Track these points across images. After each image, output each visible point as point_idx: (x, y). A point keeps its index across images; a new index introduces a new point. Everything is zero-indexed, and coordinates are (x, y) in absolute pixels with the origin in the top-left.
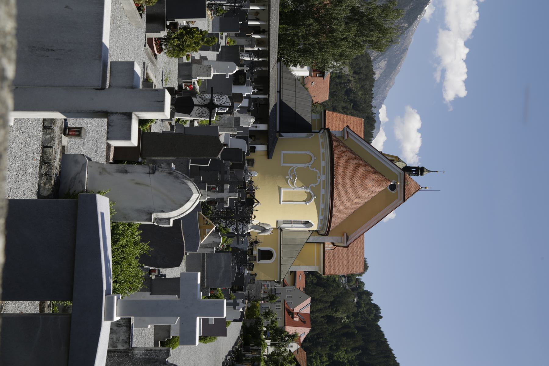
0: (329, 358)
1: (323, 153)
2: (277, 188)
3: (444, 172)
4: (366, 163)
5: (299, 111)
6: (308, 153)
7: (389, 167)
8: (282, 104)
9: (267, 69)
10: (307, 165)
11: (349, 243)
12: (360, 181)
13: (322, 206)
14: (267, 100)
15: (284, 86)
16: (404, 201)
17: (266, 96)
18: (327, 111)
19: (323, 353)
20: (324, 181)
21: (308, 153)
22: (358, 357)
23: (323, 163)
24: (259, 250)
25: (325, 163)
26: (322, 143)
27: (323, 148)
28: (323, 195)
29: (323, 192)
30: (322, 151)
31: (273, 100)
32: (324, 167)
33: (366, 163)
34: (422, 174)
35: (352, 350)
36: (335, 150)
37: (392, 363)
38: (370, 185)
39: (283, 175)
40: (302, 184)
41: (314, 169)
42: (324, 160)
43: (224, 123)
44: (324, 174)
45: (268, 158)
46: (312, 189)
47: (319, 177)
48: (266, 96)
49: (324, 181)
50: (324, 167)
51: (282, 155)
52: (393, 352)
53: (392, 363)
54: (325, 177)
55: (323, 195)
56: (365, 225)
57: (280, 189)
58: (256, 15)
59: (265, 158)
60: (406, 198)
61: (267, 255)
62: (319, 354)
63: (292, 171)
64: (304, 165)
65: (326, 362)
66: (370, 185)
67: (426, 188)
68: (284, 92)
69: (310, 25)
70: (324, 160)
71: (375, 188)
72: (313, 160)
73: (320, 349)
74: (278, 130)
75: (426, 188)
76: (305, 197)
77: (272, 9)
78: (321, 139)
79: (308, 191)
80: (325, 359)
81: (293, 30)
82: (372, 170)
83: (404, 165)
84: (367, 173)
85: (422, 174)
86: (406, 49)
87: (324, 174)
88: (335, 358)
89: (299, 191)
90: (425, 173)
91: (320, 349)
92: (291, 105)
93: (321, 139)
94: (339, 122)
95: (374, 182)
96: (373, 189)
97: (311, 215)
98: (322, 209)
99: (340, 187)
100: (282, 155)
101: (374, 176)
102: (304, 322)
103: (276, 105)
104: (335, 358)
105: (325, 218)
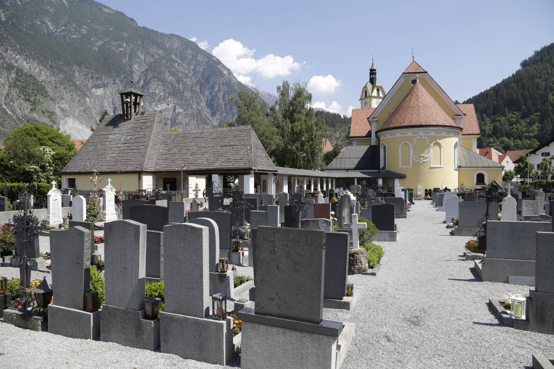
0: (491, 137)
1: (401, 134)
3: (373, 55)
5: (361, 156)
6: (400, 147)
9: (334, 179)
10: (411, 147)
11: (462, 114)
14: (360, 180)
15: (343, 167)
17: (356, 180)
19: (487, 141)
20: (424, 133)
22: (489, 116)
23: (421, 134)
24: (476, 184)
25: (409, 133)
27: (395, 135)
29: (433, 134)
30: (398, 135)
31: (358, 174)
32: (412, 133)
34: (375, 70)
35: (483, 121)
36: (397, 125)
37: (491, 92)
38: (422, 97)
39: (419, 165)
40: (427, 150)
41: (415, 141)
42: (406, 134)
43: (532, 210)
44: (418, 133)
45: (405, 177)
47: (421, 137)
48: (356, 180)
49: (424, 133)
51: (411, 164)
52: (483, 91)
53: (491, 92)
54: (421, 132)
55: (435, 133)
56: (447, 102)
57: (431, 168)
59: (405, 180)
62: (488, 144)
64: (411, 149)
65: (494, 139)
66: (422, 97)
67: (413, 57)
68: (347, 167)
71: (422, 94)
72: (407, 142)
73: (484, 144)
74: (377, 171)
76: (437, 147)
78: (387, 138)
79: (432, 145)
81: (300, 161)
82: (409, 96)
83: (369, 83)
84: (413, 100)
85: (375, 70)
86: (269, 94)
87: (418, 133)
88: (491, 133)
89: (432, 153)
90: (374, 68)
91: (484, 144)
92: (356, 161)
93: (387, 138)
94: (357, 126)
95: (419, 94)
96: (425, 95)
97: (450, 143)
98: (446, 134)
99: (428, 120)
101: (414, 95)
102: (487, 153)
103: (361, 172)
104: (491, 133)
105: (452, 132)
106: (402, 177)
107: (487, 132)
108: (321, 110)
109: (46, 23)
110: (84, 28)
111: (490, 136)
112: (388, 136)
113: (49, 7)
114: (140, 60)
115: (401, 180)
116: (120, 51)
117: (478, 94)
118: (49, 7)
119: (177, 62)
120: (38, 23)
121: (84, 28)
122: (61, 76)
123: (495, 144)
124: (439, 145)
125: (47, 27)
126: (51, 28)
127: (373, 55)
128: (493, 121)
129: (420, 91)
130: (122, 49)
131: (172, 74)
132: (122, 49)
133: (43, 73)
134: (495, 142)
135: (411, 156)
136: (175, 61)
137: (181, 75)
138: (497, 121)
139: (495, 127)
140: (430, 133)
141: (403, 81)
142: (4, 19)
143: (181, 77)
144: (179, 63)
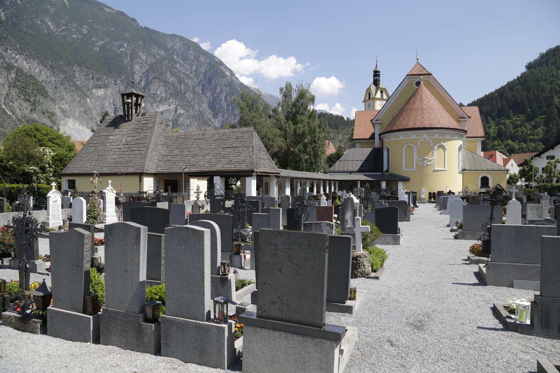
0: (495, 140)
1: (404, 137)
2: (434, 173)
3: (377, 56)
4: (408, 102)
6: (404, 149)
7: (401, 90)
8: (360, 171)
10: (415, 150)
12: (425, 107)
13: (448, 137)
14: (363, 182)
15: (346, 169)
16: (431, 74)
17: (359, 182)
18: (354, 138)
19: (492, 144)
20: (428, 136)
21: (404, 149)
22: (493, 119)
23: (425, 136)
24: (481, 188)
25: (413, 135)
26: (394, 138)
28: (440, 136)
29: (437, 136)
30: (402, 138)
31: (361, 177)
32: (416, 136)
33: (408, 102)
34: (379, 72)
36: (401, 128)
38: (426, 99)
39: (423, 168)
40: (431, 152)
41: (418, 143)
42: (410, 136)
43: (537, 214)
44: (422, 136)
45: (409, 180)
46: (435, 145)
47: (425, 139)
48: (359, 182)
49: (428, 136)
50: (416, 136)
51: (407, 170)
52: (487, 94)
54: (425, 135)
57: (435, 171)
58: (281, 189)
59: (408, 183)
60: (427, 73)
61: (485, 181)
63: (420, 161)
64: (415, 152)
65: (498, 142)
66: (426, 99)
68: (350, 169)
69: (300, 151)
70: (410, 136)
72: (411, 145)
74: (381, 173)
75: (418, 59)
76: (441, 150)
77: (309, 177)
78: (390, 140)
79: (436, 148)
80: (496, 143)
81: (303, 164)
82: (413, 98)
83: (373, 85)
84: (417, 102)
85: (379, 72)
86: (271, 96)
87: (422, 136)
88: (495, 135)
89: (436, 156)
90: (378, 70)
92: (360, 164)
93: (390, 140)
94: (361, 129)
95: (424, 96)
96: (429, 97)
97: (454, 145)
99: (432, 122)
100: (407, 170)
101: (418, 97)
103: (364, 175)
104: (495, 135)
105: (457, 134)
106: (405, 180)
107: (492, 134)
108: (324, 112)
110: (85, 28)
111: (494, 139)
112: (392, 139)
116: (122, 52)
119: (178, 62)
120: (39, 22)
121: (85, 28)
122: (62, 76)
123: (500, 147)
124: (443, 148)
126: (52, 28)
127: (377, 56)
128: (498, 124)
129: (424, 93)
130: (123, 49)
133: (43, 73)
134: (499, 145)
136: (176, 62)
137: (182, 75)
138: (501, 124)
139: (499, 129)
140: (434, 136)
141: (407, 82)
143: (183, 77)
144: (181, 64)
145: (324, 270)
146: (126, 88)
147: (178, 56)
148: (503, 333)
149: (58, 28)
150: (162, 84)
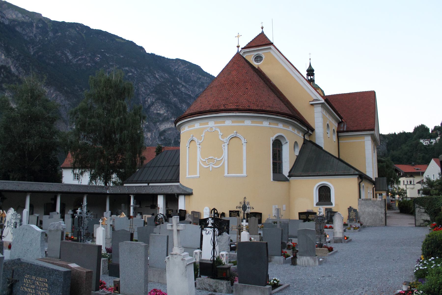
3: (262, 28)
59: (192, 197)
64: (198, 149)
109: (66, 55)
110: (98, 57)
113: (70, 41)
114: (146, 84)
115: (187, 197)
116: (129, 76)
117: (60, 21)
118: (70, 41)
119: (181, 84)
120: (59, 54)
121: (98, 57)
122: (75, 100)
125: (67, 57)
126: (70, 58)
130: (130, 74)
131: (175, 95)
132: (130, 74)
133: (58, 98)
135: (198, 160)
136: (178, 83)
137: (184, 96)
142: (32, 53)
143: (185, 98)
144: (183, 85)
145: (288, 72)
146: (77, 133)
147: (180, 78)
148: (416, 216)
149: (75, 58)
150: (165, 105)
